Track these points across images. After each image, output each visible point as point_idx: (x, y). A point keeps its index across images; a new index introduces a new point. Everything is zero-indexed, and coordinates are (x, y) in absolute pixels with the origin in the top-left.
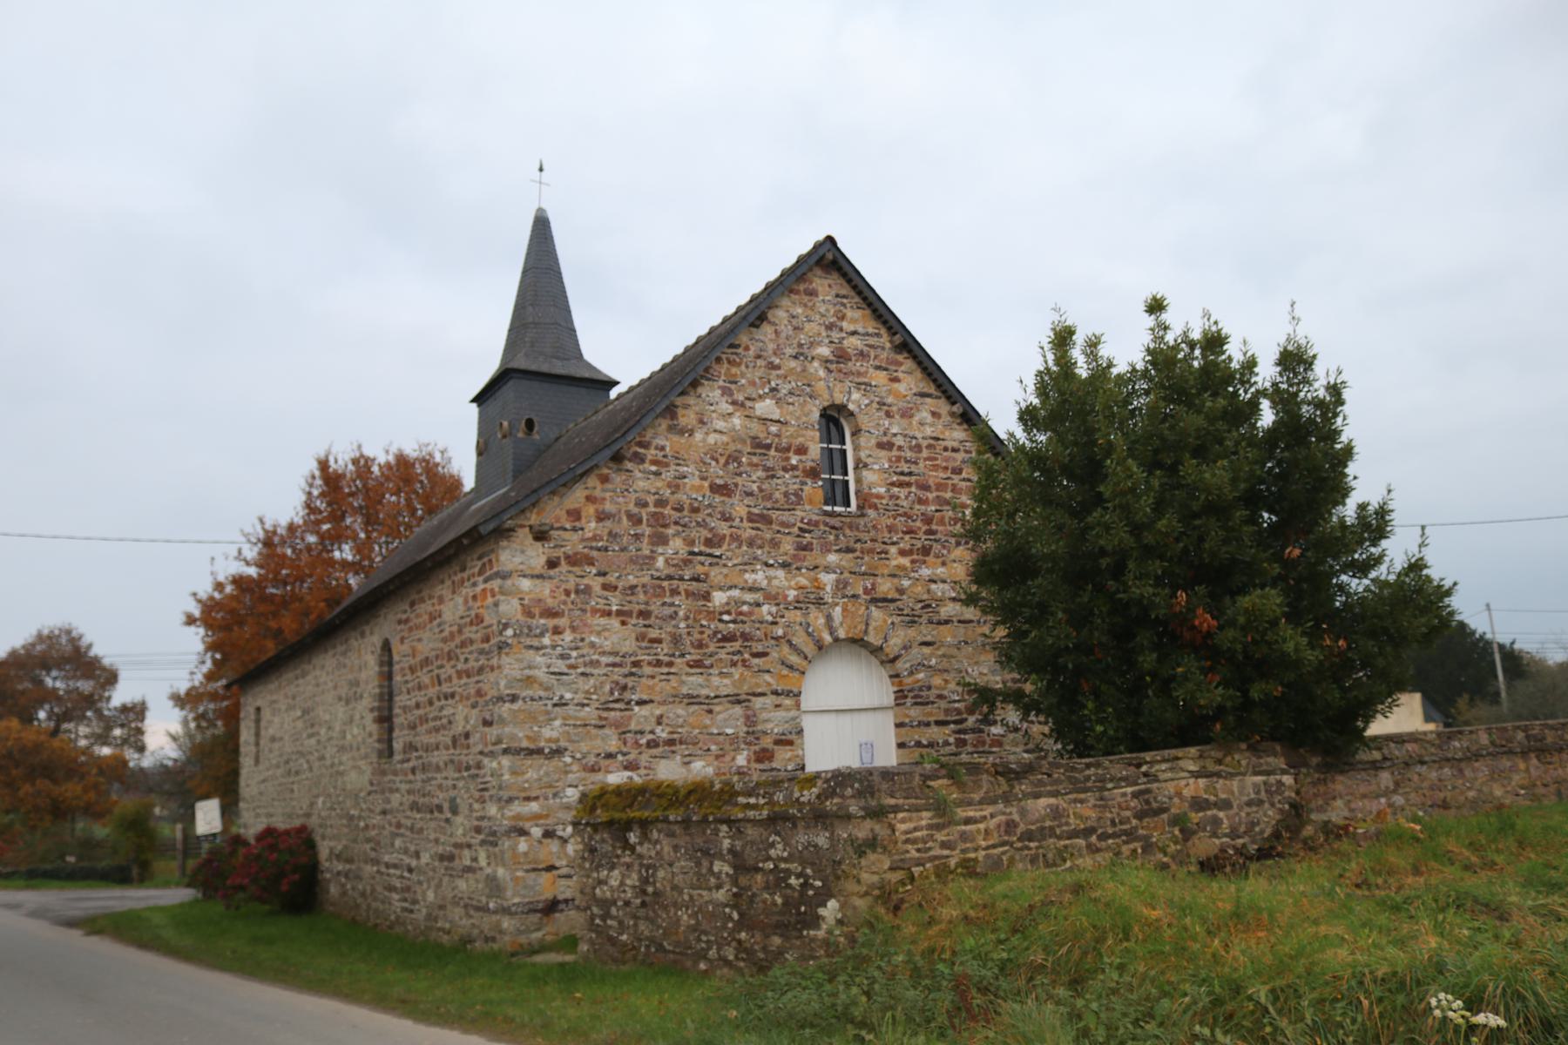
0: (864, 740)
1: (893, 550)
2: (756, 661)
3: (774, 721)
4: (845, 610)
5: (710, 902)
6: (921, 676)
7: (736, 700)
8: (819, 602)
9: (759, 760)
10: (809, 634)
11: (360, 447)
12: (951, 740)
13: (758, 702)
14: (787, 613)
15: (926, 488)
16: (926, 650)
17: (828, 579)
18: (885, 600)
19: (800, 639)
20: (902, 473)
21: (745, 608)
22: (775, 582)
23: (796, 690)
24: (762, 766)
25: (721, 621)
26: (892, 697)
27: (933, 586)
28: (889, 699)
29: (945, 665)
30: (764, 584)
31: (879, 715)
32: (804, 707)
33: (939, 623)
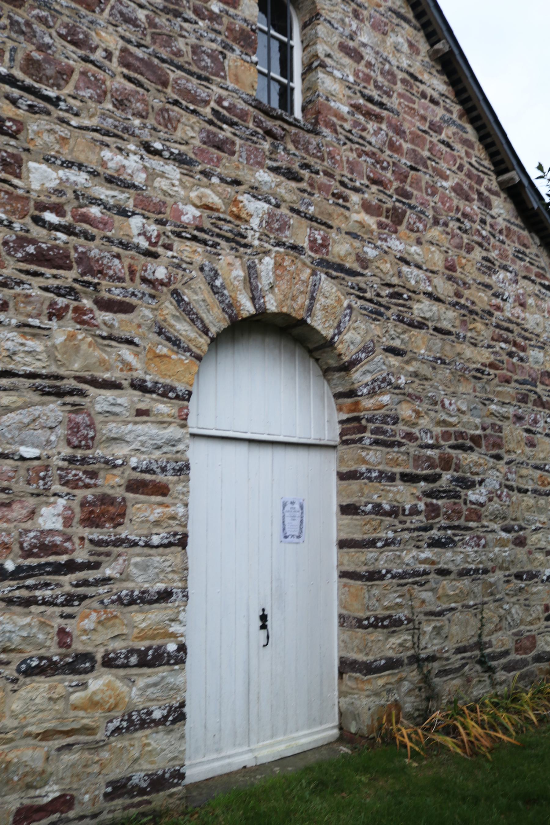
0: (289, 498)
1: (355, 198)
2: (108, 316)
3: (132, 439)
4: (278, 265)
5: (274, 273)
6: (386, 399)
7: (51, 387)
8: (238, 241)
9: (90, 521)
10: (215, 290)
11: (263, 610)
12: (421, 506)
13: (102, 400)
14: (177, 244)
15: (399, 132)
16: (394, 361)
17: (256, 208)
18: (340, 268)
19: (197, 295)
20: (370, 99)
21: (95, 211)
22: (161, 183)
23: (181, 388)
24: (96, 534)
25: (38, 220)
26: (338, 429)
27: (405, 269)
28: (331, 433)
29: (416, 388)
30: (140, 178)
31: (315, 456)
32: (194, 426)
33: (411, 324)
